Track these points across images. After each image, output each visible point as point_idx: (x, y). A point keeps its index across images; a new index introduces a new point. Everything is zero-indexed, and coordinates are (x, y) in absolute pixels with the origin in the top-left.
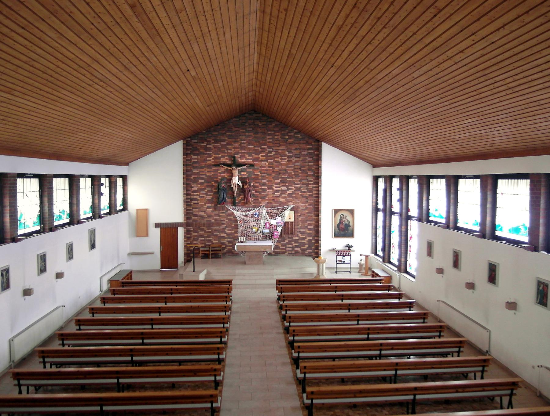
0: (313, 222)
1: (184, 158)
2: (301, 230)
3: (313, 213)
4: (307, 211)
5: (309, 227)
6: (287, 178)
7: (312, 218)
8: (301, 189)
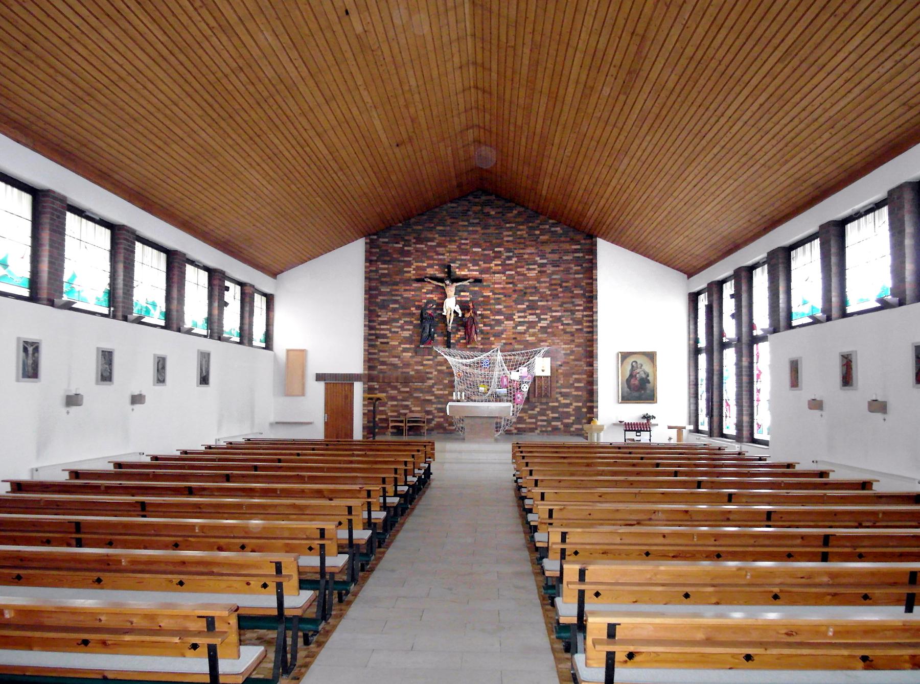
4: (572, 357)
5: (576, 385)
6: (538, 301)
8: (563, 319)
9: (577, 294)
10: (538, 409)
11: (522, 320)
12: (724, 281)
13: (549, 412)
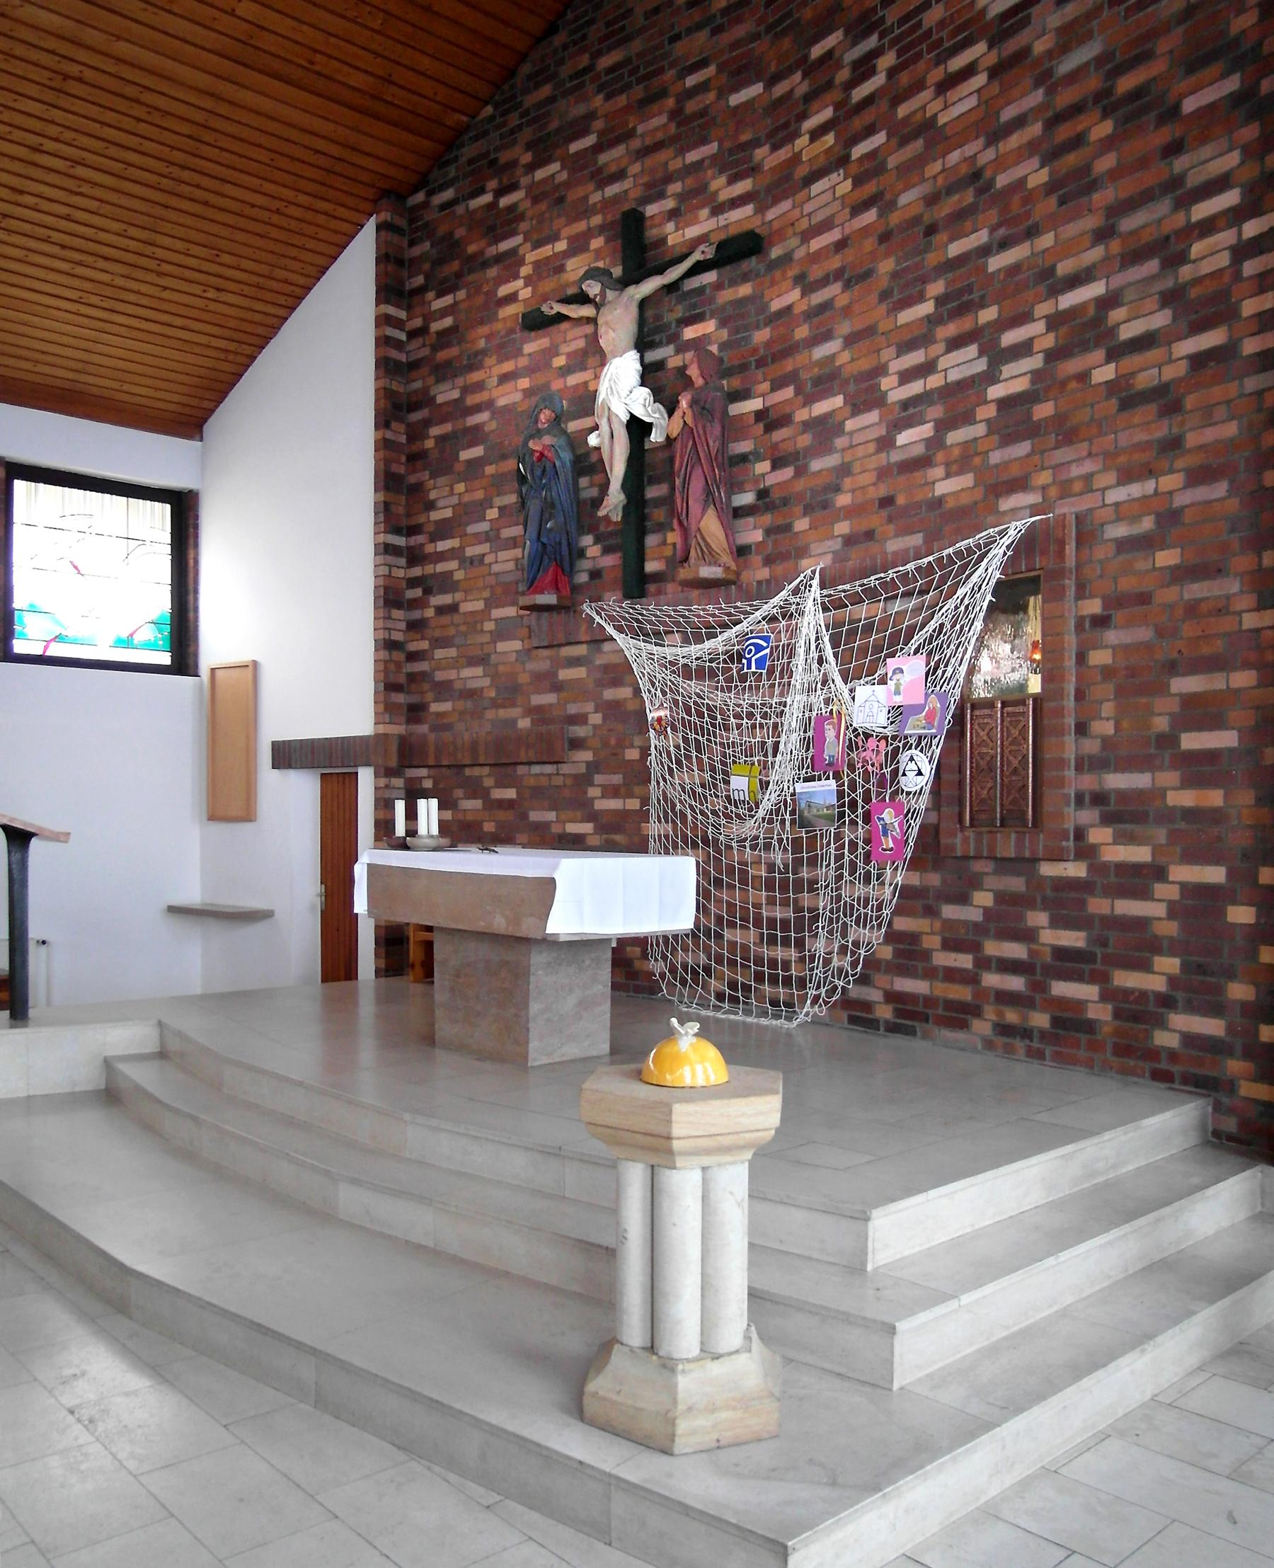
0: (1243, 679)
1: (382, 321)
2: (1117, 781)
3: (1244, 562)
4: (1167, 558)
5: (1191, 741)
6: (985, 251)
7: (1227, 624)
8: (1117, 315)
9: (1202, 112)
10: (984, 898)
11: (916, 387)
13: (1038, 918)
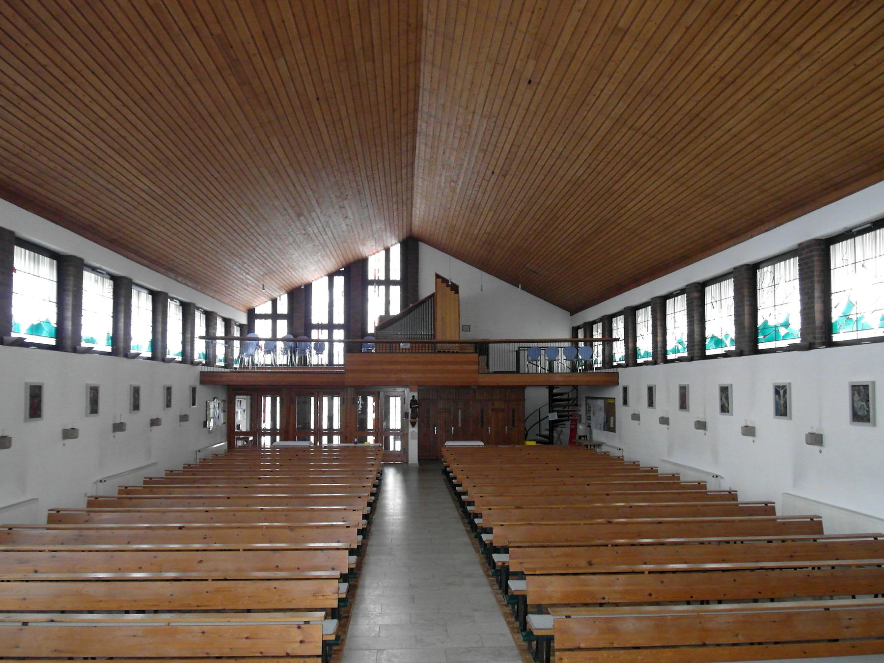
12: (595, 322)
